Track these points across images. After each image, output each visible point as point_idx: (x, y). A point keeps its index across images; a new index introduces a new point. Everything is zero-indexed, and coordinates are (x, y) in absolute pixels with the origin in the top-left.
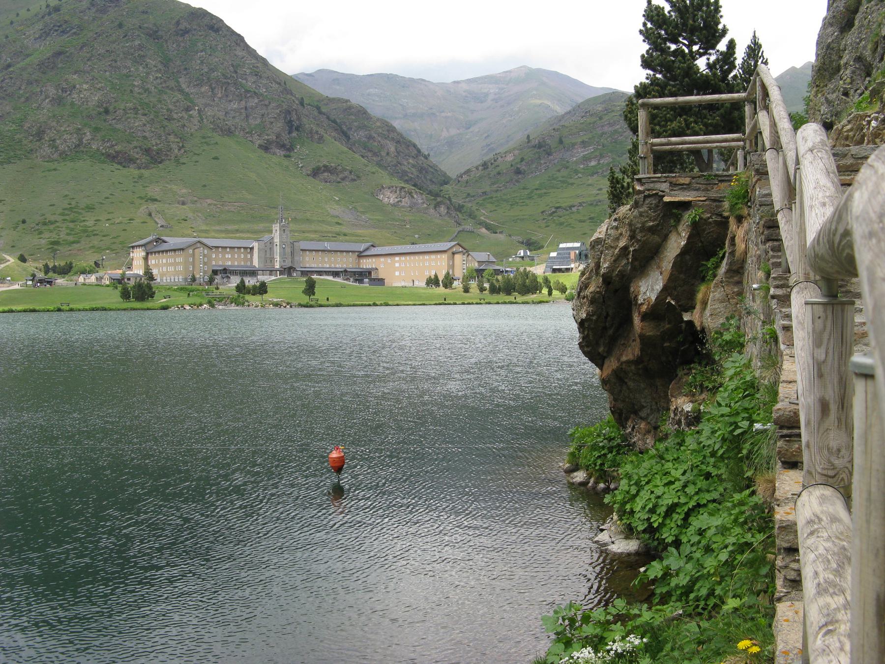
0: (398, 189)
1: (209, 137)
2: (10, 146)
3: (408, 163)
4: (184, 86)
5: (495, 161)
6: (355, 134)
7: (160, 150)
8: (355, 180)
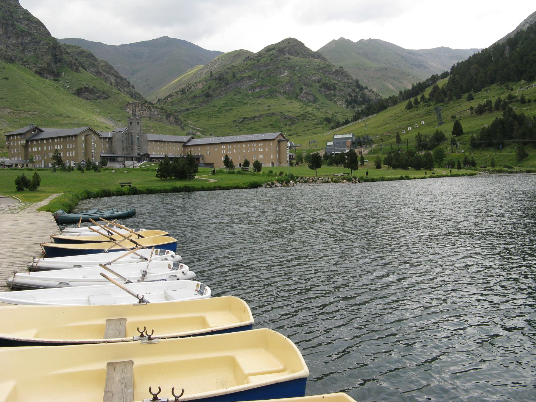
0: (140, 104)
3: (124, 91)
5: (190, 88)
8: (106, 98)
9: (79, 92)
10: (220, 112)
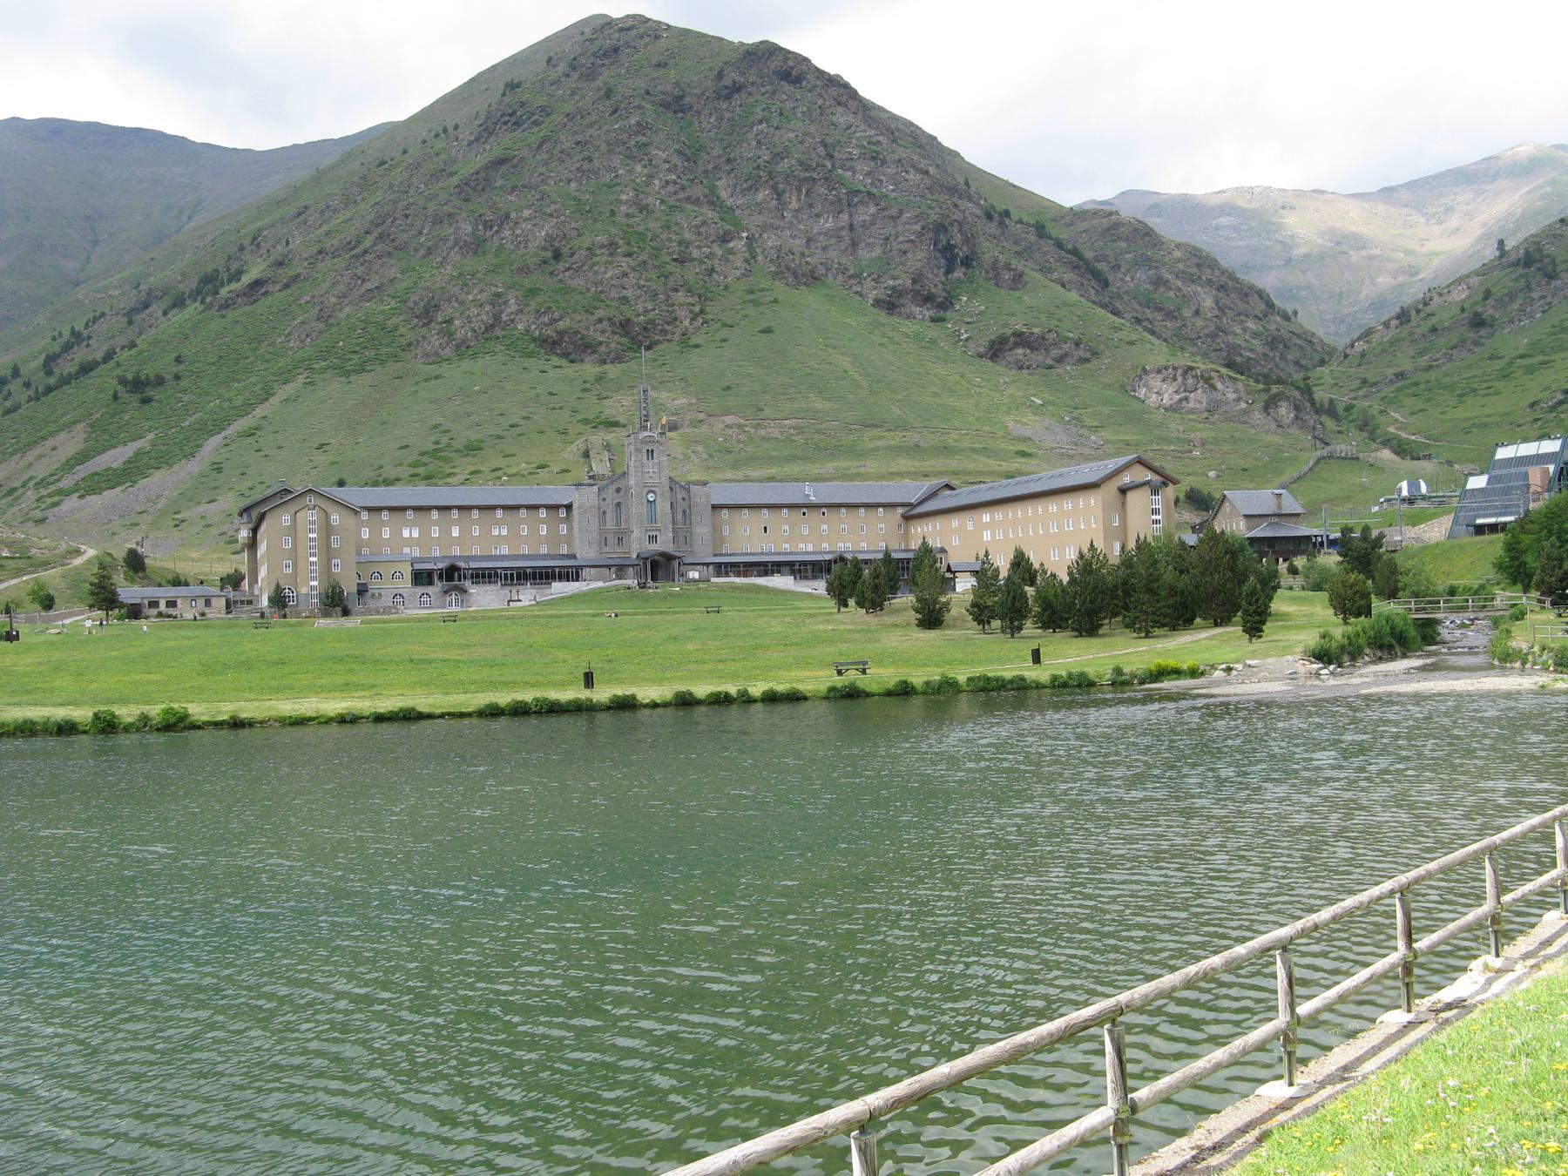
0: (1179, 372)
1: (763, 290)
2: (373, 339)
3: (1245, 330)
4: (724, 194)
6: (1128, 278)
7: (652, 322)
8: (1087, 360)
9: (996, 350)
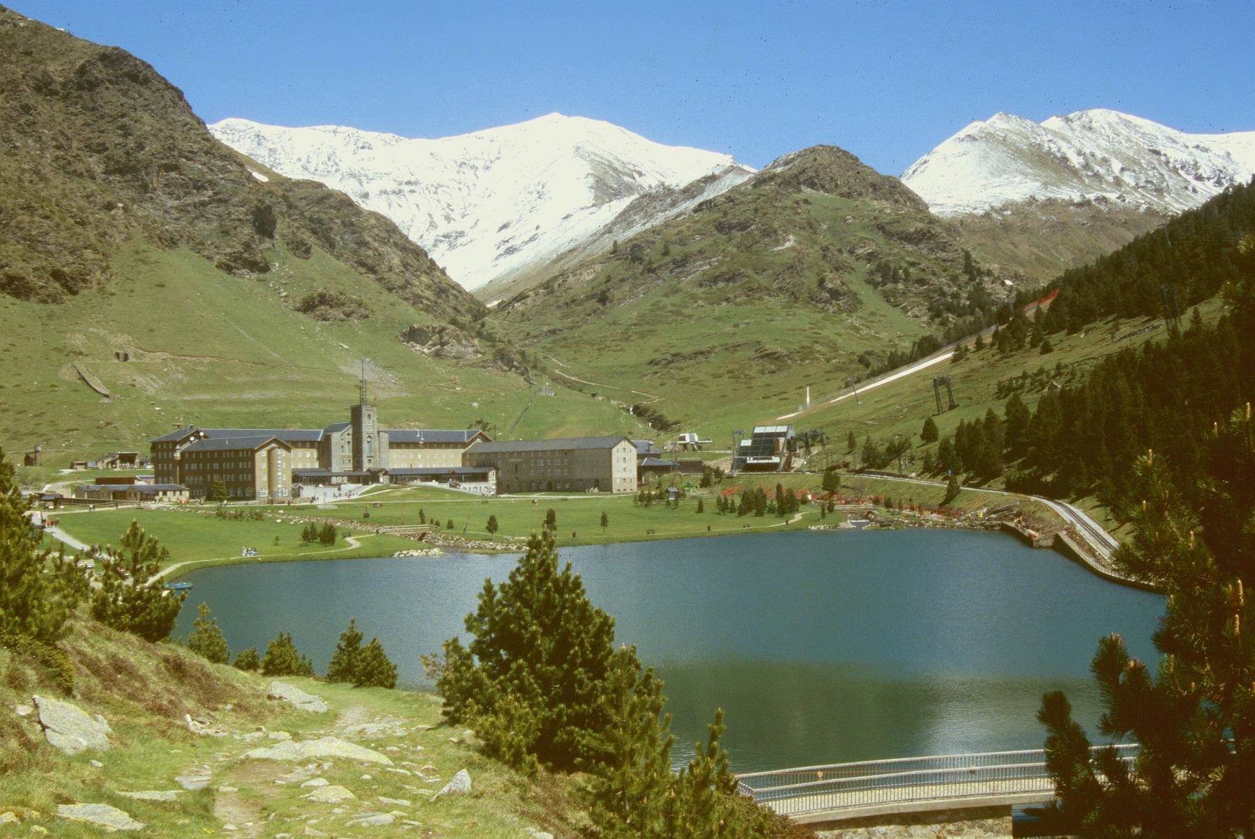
1: (144, 251)
10: (627, 339)
